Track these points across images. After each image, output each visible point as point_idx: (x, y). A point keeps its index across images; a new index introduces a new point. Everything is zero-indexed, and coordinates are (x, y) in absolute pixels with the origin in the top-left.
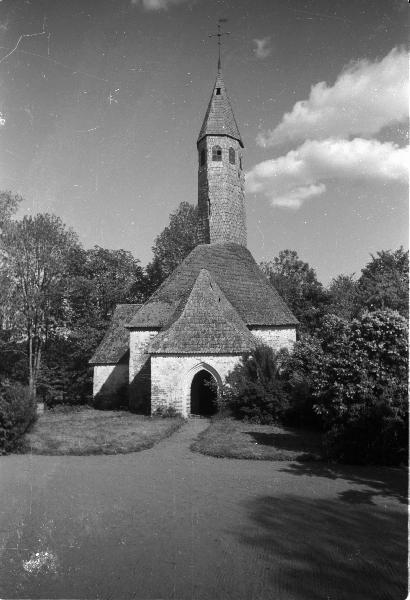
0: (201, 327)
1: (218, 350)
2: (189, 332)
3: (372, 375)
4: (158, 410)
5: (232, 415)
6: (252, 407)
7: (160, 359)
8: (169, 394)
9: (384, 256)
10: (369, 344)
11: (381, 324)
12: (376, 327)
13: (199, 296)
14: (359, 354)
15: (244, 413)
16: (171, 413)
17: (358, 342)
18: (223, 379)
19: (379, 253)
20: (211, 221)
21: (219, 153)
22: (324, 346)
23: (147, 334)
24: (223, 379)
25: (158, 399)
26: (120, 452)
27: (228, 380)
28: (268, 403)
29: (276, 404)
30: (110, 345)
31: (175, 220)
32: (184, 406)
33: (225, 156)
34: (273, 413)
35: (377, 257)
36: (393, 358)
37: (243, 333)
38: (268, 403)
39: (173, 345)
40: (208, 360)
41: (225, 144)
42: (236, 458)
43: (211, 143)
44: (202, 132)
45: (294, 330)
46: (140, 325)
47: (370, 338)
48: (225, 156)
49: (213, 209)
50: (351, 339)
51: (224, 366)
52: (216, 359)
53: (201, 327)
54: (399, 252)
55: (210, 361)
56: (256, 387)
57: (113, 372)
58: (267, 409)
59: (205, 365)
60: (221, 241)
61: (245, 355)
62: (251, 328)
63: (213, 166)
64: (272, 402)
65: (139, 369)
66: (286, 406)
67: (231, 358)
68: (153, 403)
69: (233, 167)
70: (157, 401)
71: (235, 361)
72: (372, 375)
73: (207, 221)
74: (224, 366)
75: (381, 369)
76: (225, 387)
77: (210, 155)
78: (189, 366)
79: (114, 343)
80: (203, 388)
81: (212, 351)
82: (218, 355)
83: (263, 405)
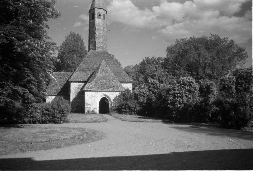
0: (104, 81)
1: (110, 90)
2: (100, 83)
3: (186, 96)
4: (88, 111)
5: (117, 112)
6: (126, 109)
7: (89, 93)
8: (92, 106)
9: (147, 58)
10: (186, 87)
11: (189, 81)
12: (187, 82)
13: (103, 70)
14: (183, 90)
15: (123, 112)
16: (93, 112)
17: (182, 86)
18: (112, 100)
19: (146, 58)
20: (97, 42)
21: (100, 15)
22: (148, 89)
23: (78, 83)
24: (112, 100)
25: (88, 107)
26: (98, 122)
27: (114, 100)
28: (132, 108)
29: (135, 108)
30: (52, 88)
31: (67, 39)
32: (97, 110)
33: (102, 17)
34: (134, 111)
35: (145, 59)
36: (193, 91)
37: (119, 84)
38: (132, 108)
39: (94, 88)
40: (106, 93)
41: (102, 12)
42: (143, 122)
43: (97, 11)
44: (92, 6)
45: (132, 84)
46: (75, 80)
47: (185, 85)
48: (102, 17)
49: (97, 37)
50: (179, 85)
51: (112, 96)
52: (110, 93)
53: (104, 81)
54: (153, 58)
55: (107, 94)
56: (128, 103)
57: (55, 98)
58: (132, 110)
59: (105, 95)
60: (101, 50)
61: (122, 92)
62: (121, 82)
63: (97, 20)
64: (134, 107)
65: (74, 97)
66: (138, 108)
67: (115, 93)
68: (86, 109)
69: (105, 21)
70: (88, 108)
71: (118, 94)
72: (186, 96)
73: (95, 42)
74: (112, 96)
75: (189, 94)
76: (111, 104)
77: (96, 16)
78: (99, 96)
79: (54, 87)
80: (104, 105)
81: (108, 90)
82: (110, 91)
83: (129, 108)
